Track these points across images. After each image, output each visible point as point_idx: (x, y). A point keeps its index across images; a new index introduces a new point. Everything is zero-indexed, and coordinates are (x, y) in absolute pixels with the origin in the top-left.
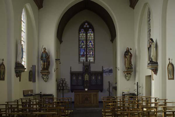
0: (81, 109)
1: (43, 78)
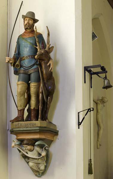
0: (40, 107)
1: (25, 157)
